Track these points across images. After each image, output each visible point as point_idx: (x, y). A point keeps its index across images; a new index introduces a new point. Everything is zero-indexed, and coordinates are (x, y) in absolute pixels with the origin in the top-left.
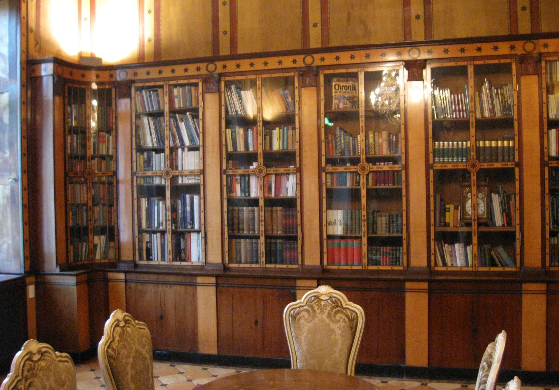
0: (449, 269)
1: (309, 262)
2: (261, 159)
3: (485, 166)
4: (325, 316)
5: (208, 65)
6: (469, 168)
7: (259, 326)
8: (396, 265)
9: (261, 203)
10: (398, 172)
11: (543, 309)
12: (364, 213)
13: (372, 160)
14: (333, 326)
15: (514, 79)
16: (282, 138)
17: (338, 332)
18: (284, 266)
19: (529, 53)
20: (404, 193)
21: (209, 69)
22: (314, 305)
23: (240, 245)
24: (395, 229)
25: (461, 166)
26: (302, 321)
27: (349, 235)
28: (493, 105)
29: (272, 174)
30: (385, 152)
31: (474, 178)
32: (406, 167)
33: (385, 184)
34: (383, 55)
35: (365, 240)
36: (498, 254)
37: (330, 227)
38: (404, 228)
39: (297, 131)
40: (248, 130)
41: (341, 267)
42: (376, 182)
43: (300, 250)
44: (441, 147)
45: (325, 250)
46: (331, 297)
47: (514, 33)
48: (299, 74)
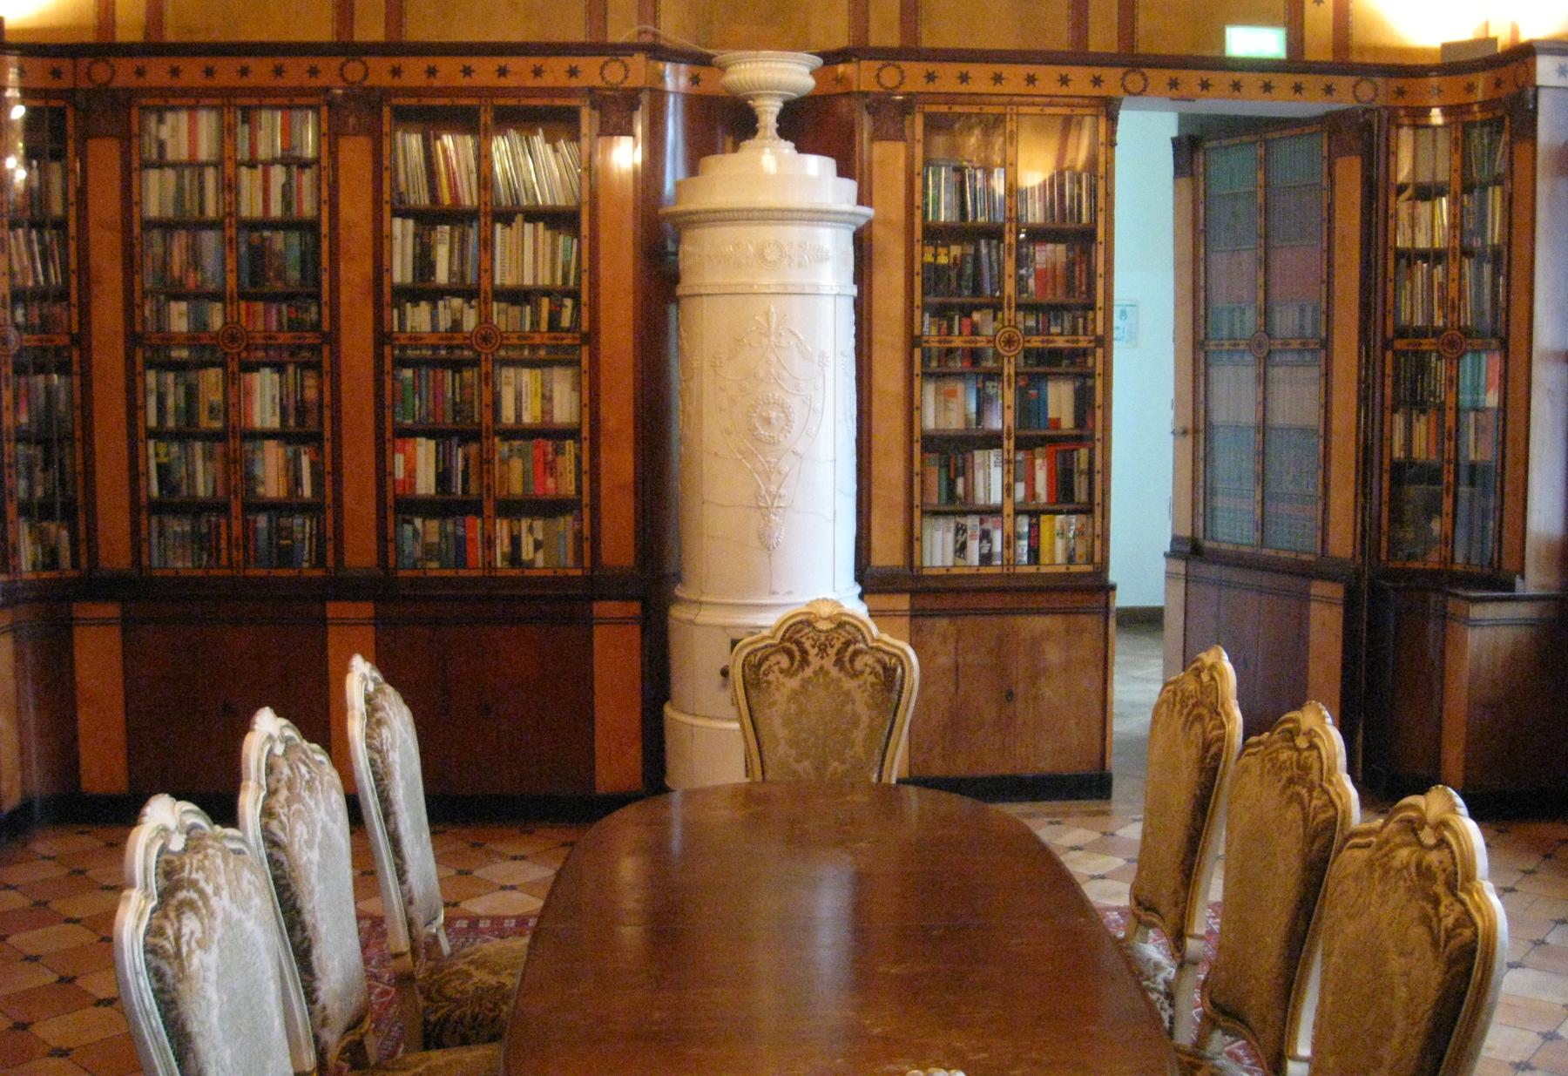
0: (1043, 570)
4: (828, 663)
5: (1125, 74)
19: (891, 92)
21: (349, 76)
22: (804, 640)
47: (155, 39)
48: (592, 103)
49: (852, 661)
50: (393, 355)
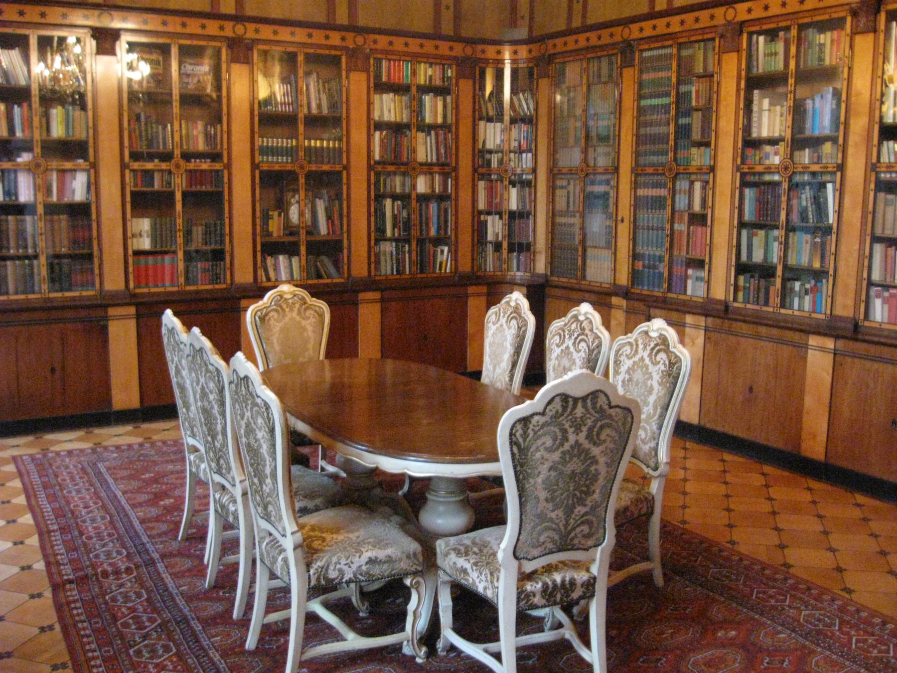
1: (109, 286)
2: (38, 150)
3: (314, 168)
4: (295, 314)
6: (298, 170)
7: (58, 373)
8: (217, 283)
9: (40, 210)
10: (217, 171)
11: (378, 316)
12: (179, 221)
13: (187, 156)
14: (304, 323)
15: (344, 73)
16: (68, 122)
17: (310, 328)
18: (76, 294)
20: (226, 197)
23: (6, 270)
24: (213, 240)
25: (289, 167)
26: (272, 322)
27: (158, 248)
28: (320, 99)
29: (52, 170)
30: (201, 146)
31: (302, 181)
32: (229, 166)
33: (196, 185)
34: (859, 94)
35: (181, 255)
36: (323, 265)
37: (135, 240)
38: (227, 239)
39: (90, 113)
40: (13, 108)
41: (154, 290)
42: (190, 183)
43: (97, 271)
44: (265, 144)
45: (131, 269)
46: (295, 295)
49: (598, 435)
50: (297, 139)
